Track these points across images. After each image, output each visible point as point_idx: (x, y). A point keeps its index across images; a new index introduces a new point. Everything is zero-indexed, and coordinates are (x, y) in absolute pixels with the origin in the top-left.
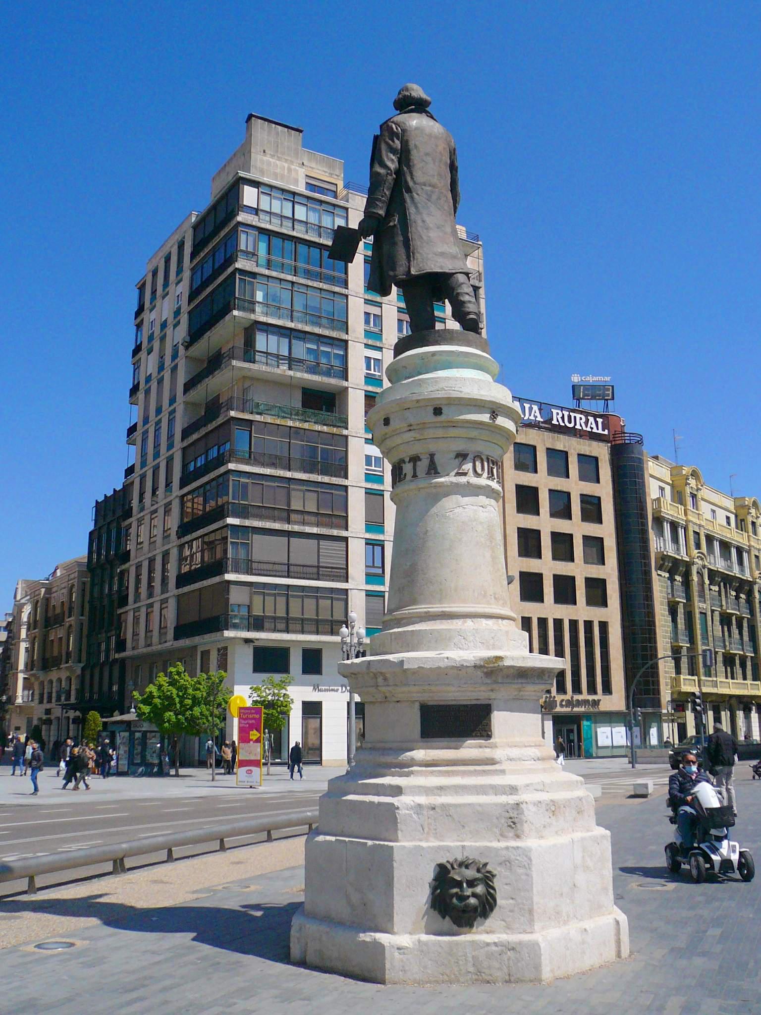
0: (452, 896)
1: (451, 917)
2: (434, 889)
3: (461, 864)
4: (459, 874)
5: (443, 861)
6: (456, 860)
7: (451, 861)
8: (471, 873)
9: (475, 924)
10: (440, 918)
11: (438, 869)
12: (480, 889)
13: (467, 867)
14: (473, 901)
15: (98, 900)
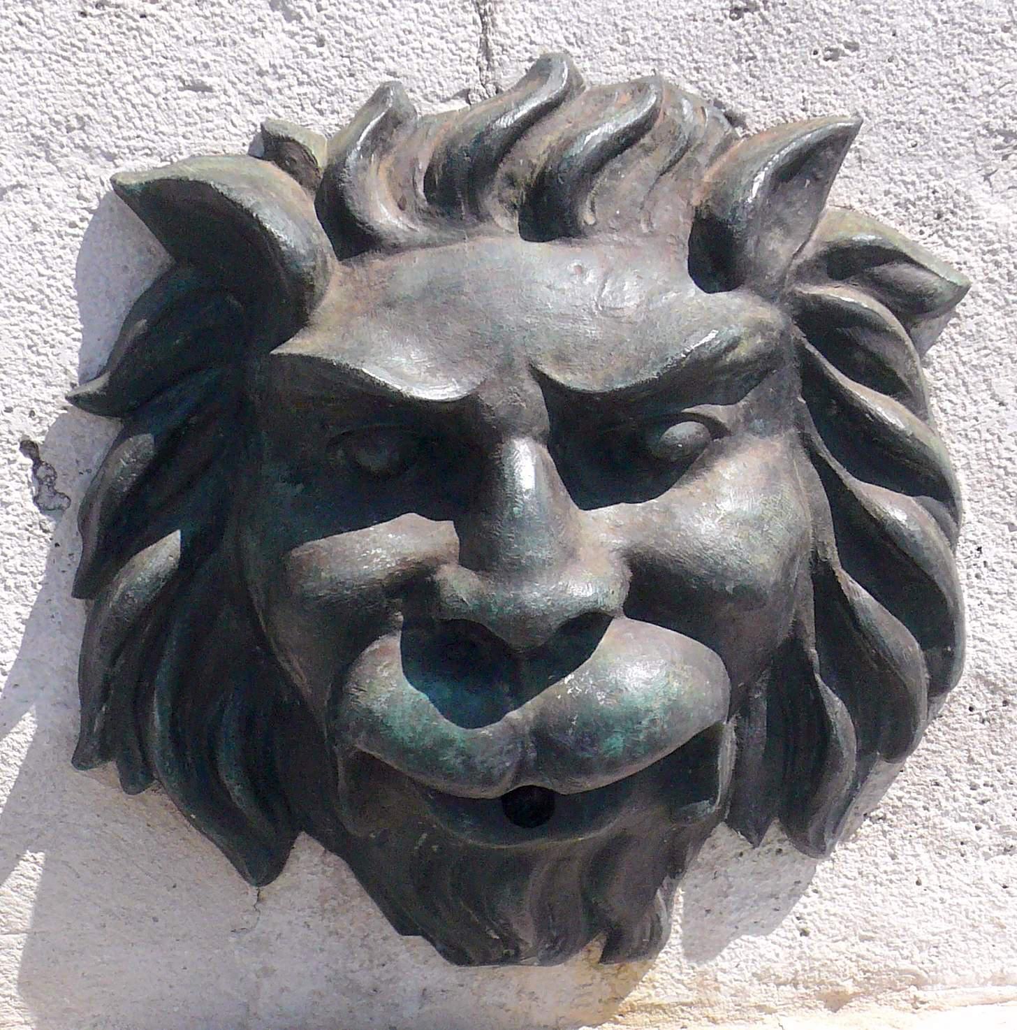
0: (354, 620)
1: (341, 845)
2: (109, 530)
3: (459, 183)
4: (433, 313)
5: (207, 141)
6: (387, 121)
7: (319, 126)
8: (612, 299)
9: (679, 907)
10: (203, 862)
11: (139, 258)
12: (740, 504)
13: (550, 212)
14: (647, 675)
15: (730, 357)
